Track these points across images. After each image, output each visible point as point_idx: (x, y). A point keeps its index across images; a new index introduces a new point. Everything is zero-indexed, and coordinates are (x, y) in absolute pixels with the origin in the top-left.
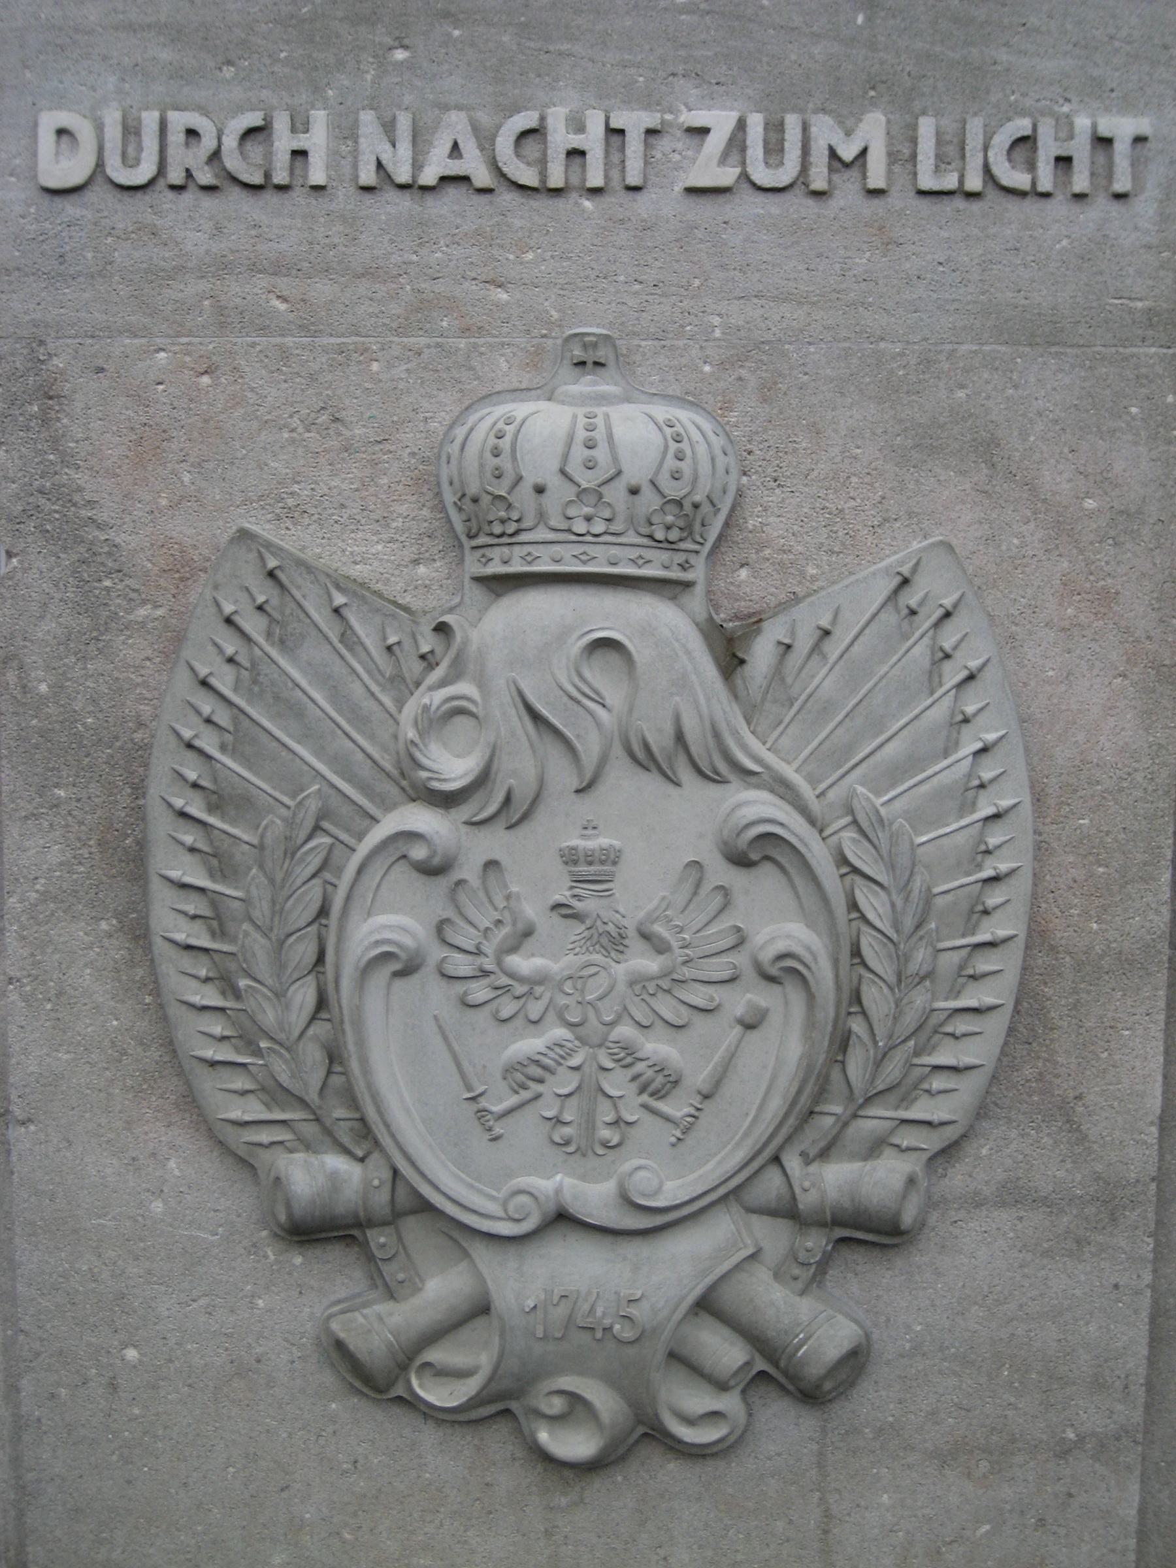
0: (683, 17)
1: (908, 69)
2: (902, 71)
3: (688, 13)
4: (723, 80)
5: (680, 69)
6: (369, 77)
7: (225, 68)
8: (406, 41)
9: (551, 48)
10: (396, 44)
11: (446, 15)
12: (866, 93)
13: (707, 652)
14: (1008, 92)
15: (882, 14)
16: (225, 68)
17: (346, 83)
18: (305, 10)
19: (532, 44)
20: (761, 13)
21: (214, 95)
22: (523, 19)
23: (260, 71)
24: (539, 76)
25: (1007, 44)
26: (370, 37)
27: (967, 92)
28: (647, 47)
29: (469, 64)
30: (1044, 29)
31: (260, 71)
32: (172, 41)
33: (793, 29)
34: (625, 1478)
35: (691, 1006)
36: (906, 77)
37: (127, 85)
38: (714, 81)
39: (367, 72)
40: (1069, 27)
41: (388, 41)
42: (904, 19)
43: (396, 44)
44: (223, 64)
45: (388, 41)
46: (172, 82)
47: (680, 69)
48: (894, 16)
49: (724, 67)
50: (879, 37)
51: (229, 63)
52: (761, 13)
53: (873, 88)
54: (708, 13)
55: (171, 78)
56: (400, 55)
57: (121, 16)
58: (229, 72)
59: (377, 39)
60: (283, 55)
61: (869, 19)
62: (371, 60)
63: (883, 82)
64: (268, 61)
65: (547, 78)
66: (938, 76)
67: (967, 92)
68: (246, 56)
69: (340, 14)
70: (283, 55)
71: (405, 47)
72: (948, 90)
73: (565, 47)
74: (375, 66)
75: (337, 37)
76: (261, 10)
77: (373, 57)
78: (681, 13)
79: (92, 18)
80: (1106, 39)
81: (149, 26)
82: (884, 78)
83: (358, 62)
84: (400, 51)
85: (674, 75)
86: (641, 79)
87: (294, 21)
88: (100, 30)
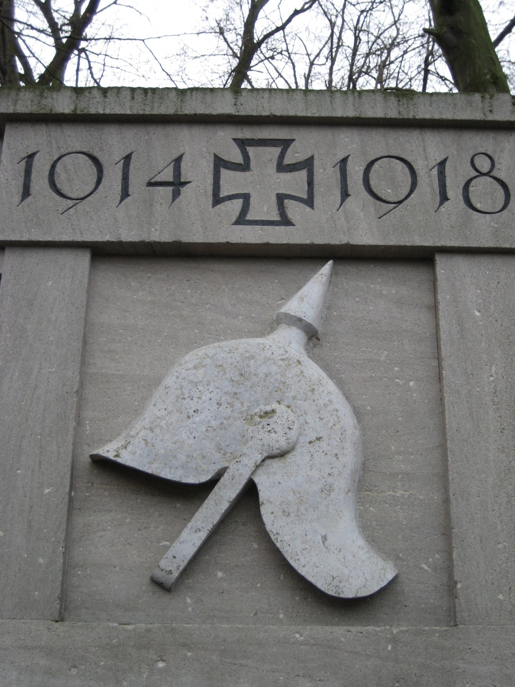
0: (302, 647)
1: (414, 672)
2: (412, 673)
3: (304, 645)
4: (322, 678)
5: (301, 673)
6: (145, 676)
7: (72, 669)
8: (164, 658)
9: (236, 662)
10: (159, 659)
11: (185, 645)
12: (395, 684)
13: (222, 516)
14: (465, 683)
15: (400, 645)
16: (72, 669)
17: (133, 678)
18: (114, 641)
19: (227, 660)
20: (341, 645)
21: (66, 683)
22: (223, 647)
23: (90, 671)
24: (230, 676)
25: (462, 659)
26: (146, 655)
27: (445, 683)
28: (285, 662)
29: (195, 670)
30: (480, 650)
31: (90, 671)
32: (47, 655)
33: (357, 653)
34: (445, 371)
35: (447, 514)
36: (414, 676)
37: (22, 677)
38: (318, 679)
39: (144, 673)
40: (492, 650)
41: (155, 657)
42: (411, 647)
43: (159, 659)
44: (72, 667)
45: (155, 657)
46: (45, 675)
47: (301, 673)
48: (406, 646)
49: (323, 672)
50: (399, 656)
51: (75, 667)
52: (341, 645)
53: (398, 682)
54: (314, 645)
55: (45, 674)
56: (161, 665)
57: (22, 642)
58: (74, 671)
59: (150, 656)
60: (102, 663)
61: (394, 648)
62: (146, 667)
63: (402, 679)
64: (94, 667)
65: (234, 678)
66: (429, 676)
67: (445, 683)
68: (84, 663)
69: (132, 644)
70: (102, 663)
71: (164, 661)
72: (435, 682)
73: (243, 662)
74: (148, 670)
75: (130, 655)
76: (92, 641)
77: (148, 665)
78: (301, 645)
79: (8, 642)
80: (511, 655)
81: (36, 647)
82: (403, 677)
83: (140, 668)
84: (160, 662)
85: (298, 676)
86: (282, 678)
87: (108, 647)
88: (11, 648)
